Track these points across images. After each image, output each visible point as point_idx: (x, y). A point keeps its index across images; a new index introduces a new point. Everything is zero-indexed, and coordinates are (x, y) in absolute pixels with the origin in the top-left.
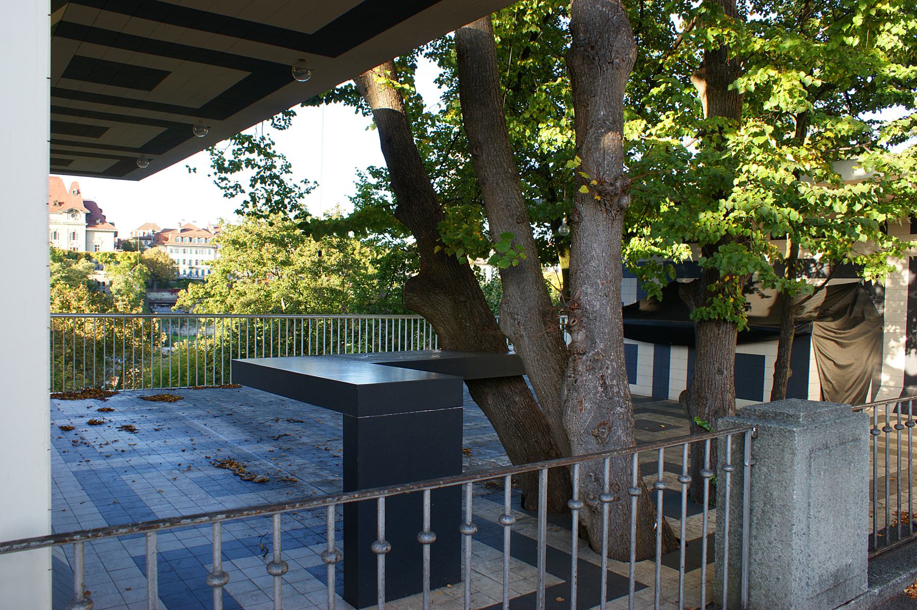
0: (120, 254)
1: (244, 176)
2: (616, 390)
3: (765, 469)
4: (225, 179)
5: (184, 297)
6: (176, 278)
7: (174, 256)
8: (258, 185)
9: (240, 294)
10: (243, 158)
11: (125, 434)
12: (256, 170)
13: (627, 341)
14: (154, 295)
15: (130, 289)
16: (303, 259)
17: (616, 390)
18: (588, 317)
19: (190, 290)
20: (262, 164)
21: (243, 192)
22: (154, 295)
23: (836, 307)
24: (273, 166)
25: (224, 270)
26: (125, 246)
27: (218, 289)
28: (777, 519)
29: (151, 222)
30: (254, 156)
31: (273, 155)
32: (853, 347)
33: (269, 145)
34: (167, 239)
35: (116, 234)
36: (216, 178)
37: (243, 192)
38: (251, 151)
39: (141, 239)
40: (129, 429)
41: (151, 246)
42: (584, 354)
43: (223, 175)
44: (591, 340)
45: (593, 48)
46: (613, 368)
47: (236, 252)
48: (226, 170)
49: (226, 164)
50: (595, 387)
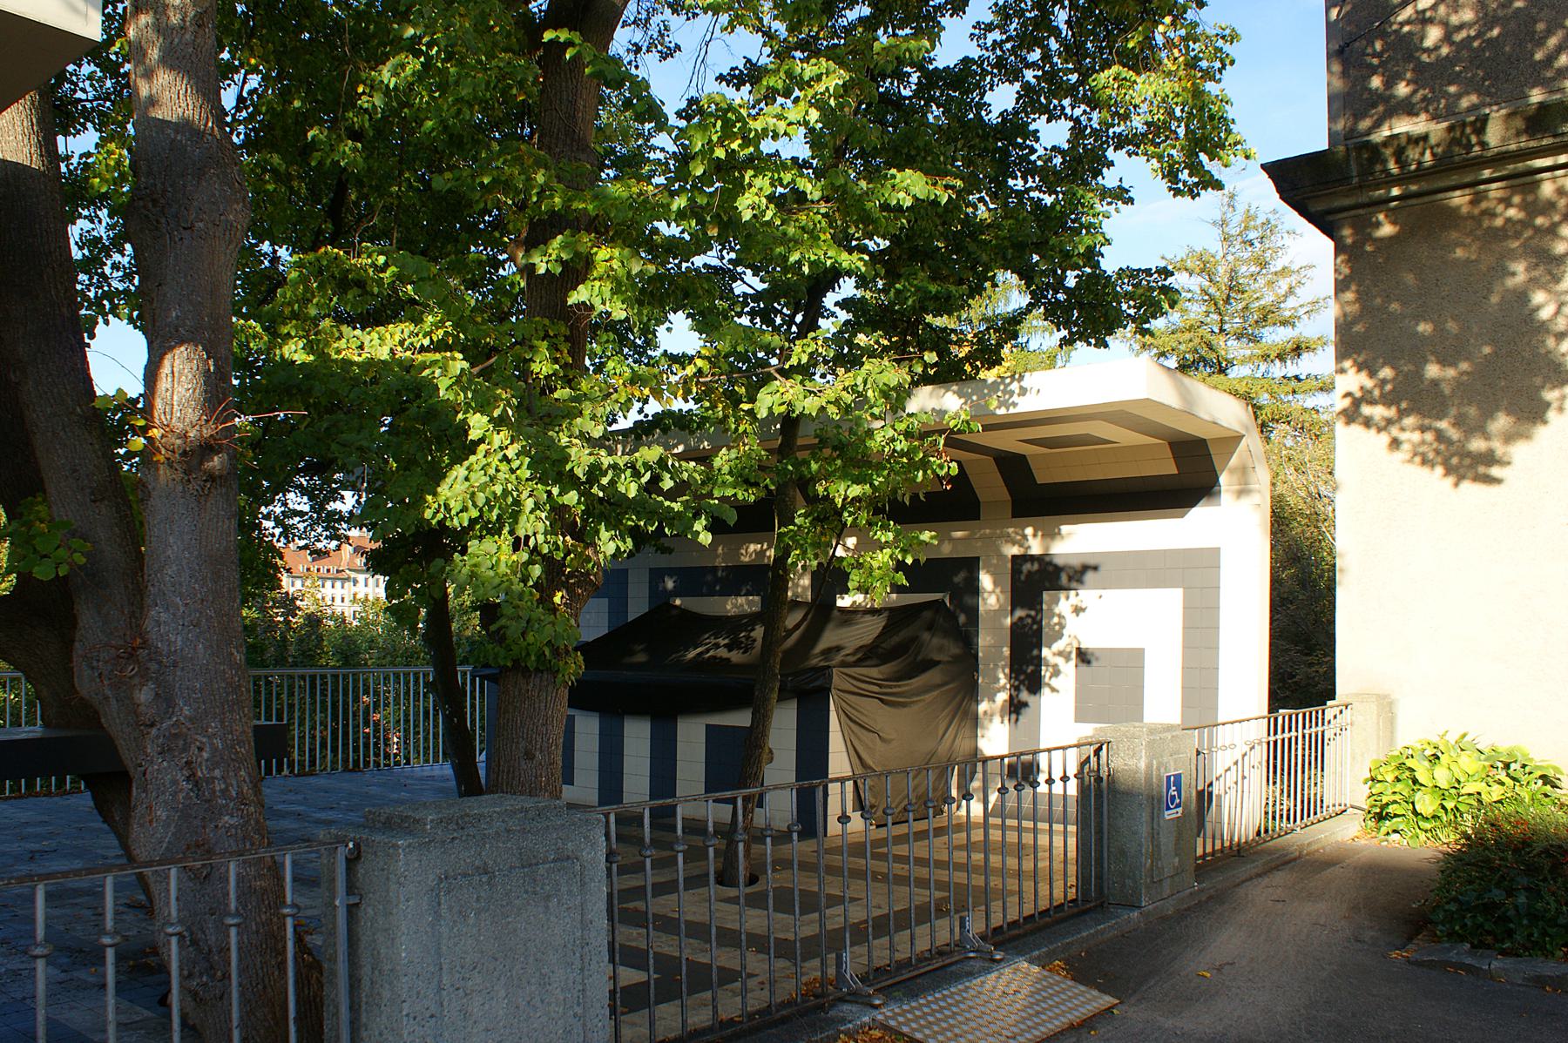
3: (370, 910)
18: (160, 663)
23: (896, 639)
28: (386, 994)
32: (915, 708)
42: (152, 725)
44: (166, 699)
45: (155, 202)
46: (214, 749)
50: (175, 782)
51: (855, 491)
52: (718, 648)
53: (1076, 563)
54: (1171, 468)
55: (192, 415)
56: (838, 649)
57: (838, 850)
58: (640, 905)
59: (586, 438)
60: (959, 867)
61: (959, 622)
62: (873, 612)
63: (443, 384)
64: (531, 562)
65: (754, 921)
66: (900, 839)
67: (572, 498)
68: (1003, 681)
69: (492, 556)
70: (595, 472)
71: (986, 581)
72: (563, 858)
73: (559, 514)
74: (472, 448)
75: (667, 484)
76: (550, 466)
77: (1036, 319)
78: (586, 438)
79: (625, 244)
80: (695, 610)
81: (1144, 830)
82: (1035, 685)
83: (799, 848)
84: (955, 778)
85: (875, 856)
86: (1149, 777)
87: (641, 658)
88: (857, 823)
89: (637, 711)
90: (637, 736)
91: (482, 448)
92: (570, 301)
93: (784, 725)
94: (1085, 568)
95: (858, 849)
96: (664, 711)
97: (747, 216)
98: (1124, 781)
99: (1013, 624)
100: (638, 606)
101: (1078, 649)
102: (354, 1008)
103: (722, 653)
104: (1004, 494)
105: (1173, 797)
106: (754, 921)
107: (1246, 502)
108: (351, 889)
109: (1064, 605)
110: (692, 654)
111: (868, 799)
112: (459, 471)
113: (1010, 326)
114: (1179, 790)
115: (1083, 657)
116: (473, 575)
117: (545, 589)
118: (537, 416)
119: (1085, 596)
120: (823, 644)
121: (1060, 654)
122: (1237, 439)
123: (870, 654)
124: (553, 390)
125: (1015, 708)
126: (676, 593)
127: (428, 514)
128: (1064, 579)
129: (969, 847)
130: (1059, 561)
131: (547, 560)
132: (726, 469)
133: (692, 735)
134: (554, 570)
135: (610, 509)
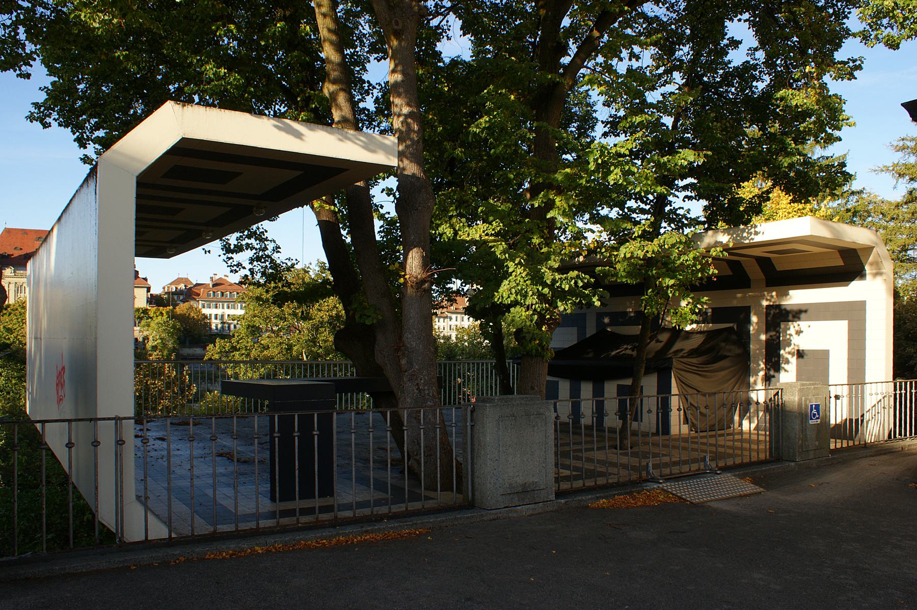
0: (152, 310)
1: (244, 257)
2: (427, 392)
4: (232, 258)
5: (213, 351)
6: (209, 333)
7: (206, 311)
8: (255, 263)
9: (264, 347)
10: (244, 243)
11: (160, 442)
12: (254, 251)
13: (549, 378)
14: (186, 351)
15: (164, 345)
16: (321, 314)
17: (427, 392)
19: (217, 345)
20: (258, 247)
21: (244, 268)
22: (186, 351)
24: (266, 249)
25: (249, 326)
26: (154, 300)
27: (243, 343)
28: (483, 453)
29: (183, 276)
30: (252, 241)
31: (266, 239)
33: (262, 232)
34: (198, 295)
35: (149, 290)
36: (225, 257)
37: (244, 268)
38: (249, 237)
39: (173, 293)
40: (162, 439)
41: (184, 301)
43: (230, 255)
44: (410, 363)
47: (260, 308)
48: (232, 252)
49: (232, 247)
51: (672, 282)
52: (627, 350)
53: (795, 308)
54: (840, 263)
55: (419, 271)
56: (682, 350)
57: (677, 440)
58: (580, 454)
59: (551, 268)
60: (729, 447)
61: (742, 338)
62: (701, 332)
63: (498, 253)
64: (533, 314)
65: (624, 460)
66: (702, 437)
67: (546, 290)
68: (762, 366)
69: (519, 314)
70: (554, 281)
71: (754, 319)
72: (539, 414)
73: (542, 297)
74: (511, 274)
75: (580, 284)
76: (537, 278)
77: (776, 193)
78: (551, 268)
79: (504, 305)
80: (617, 332)
81: (797, 427)
82: (778, 369)
83: (660, 439)
84: (737, 412)
85: (692, 442)
86: (800, 405)
87: (591, 355)
88: (685, 429)
89: (587, 379)
90: (587, 389)
91: (514, 274)
92: (548, 217)
93: (650, 384)
94: (800, 312)
95: (685, 440)
96: (598, 378)
97: (612, 183)
98: (789, 407)
99: (767, 341)
100: (591, 331)
101: (798, 351)
102: (473, 471)
103: (629, 352)
104: (761, 276)
105: (814, 415)
106: (624, 460)
107: (879, 280)
108: (472, 421)
109: (793, 327)
110: (613, 353)
111: (689, 417)
112: (506, 282)
113: (764, 197)
114: (818, 411)
115: (800, 354)
116: (513, 321)
117: (539, 324)
118: (534, 261)
119: (803, 324)
120: (674, 348)
121: (789, 353)
122: (869, 249)
123: (694, 353)
124: (541, 249)
125: (768, 379)
126: (609, 325)
127: (496, 300)
128: (790, 317)
129: (742, 441)
130: (788, 308)
131: (539, 314)
132: (622, 269)
133: (611, 388)
134: (542, 320)
135: (562, 295)
